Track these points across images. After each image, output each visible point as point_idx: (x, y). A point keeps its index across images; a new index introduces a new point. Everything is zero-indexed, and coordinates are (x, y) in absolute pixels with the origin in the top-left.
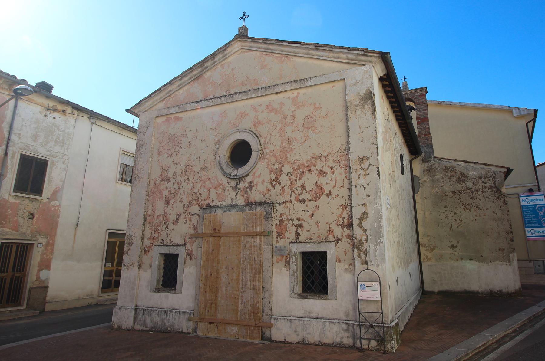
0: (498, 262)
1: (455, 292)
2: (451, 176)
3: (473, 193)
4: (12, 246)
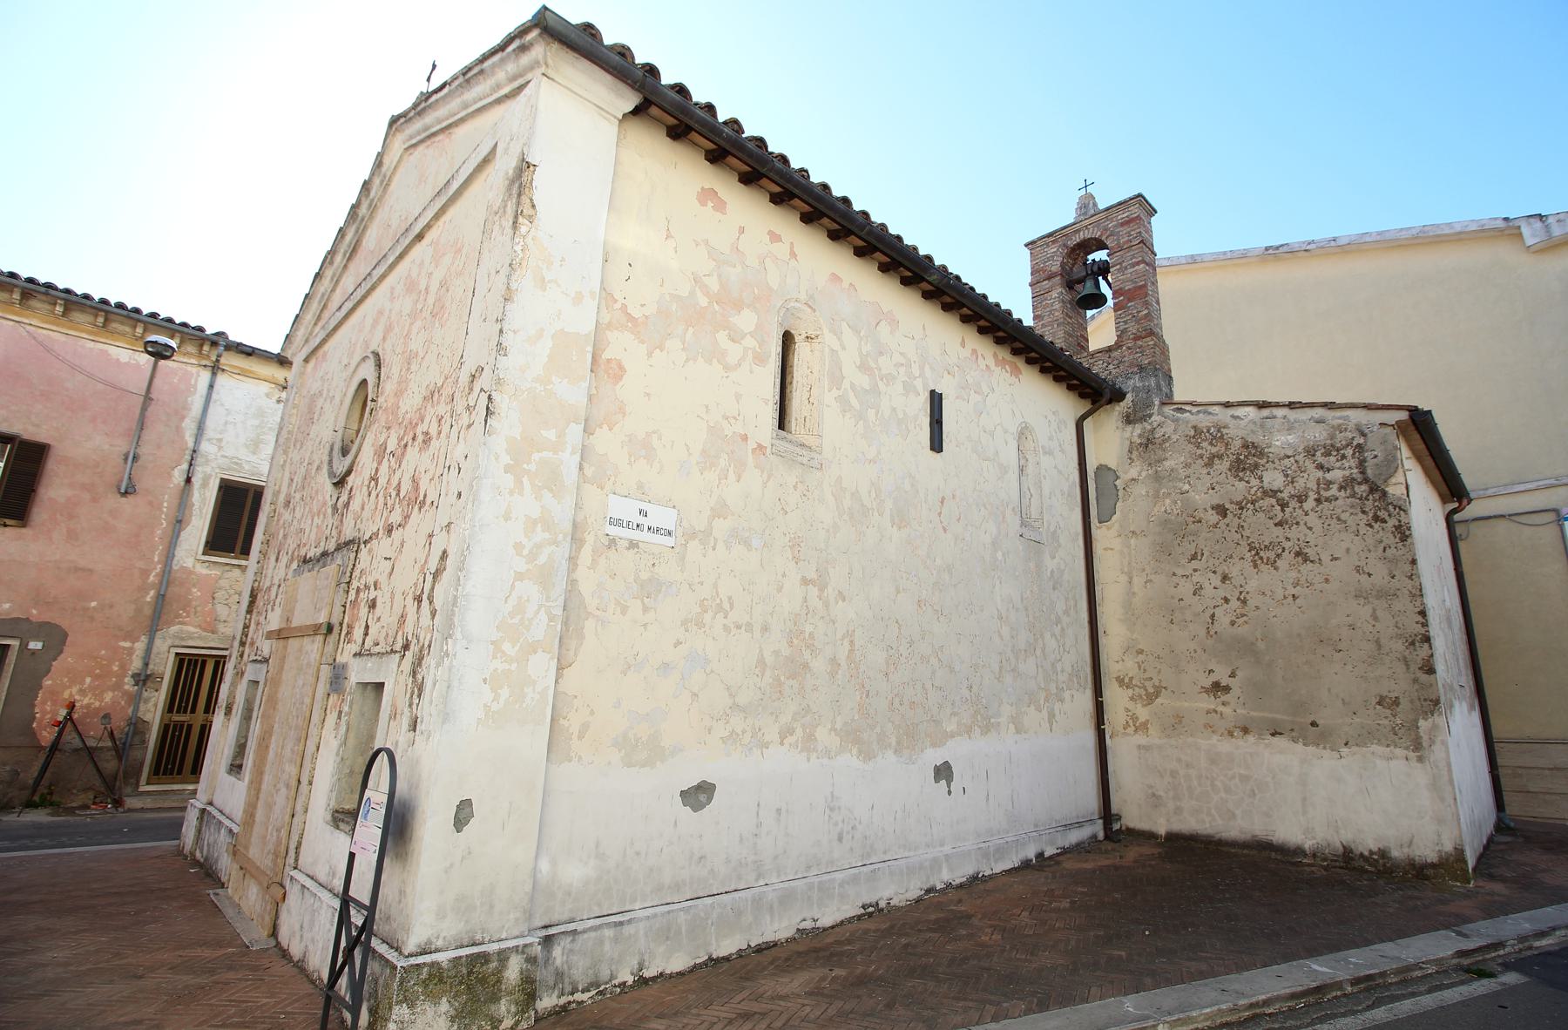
0: (1374, 748)
1: (1221, 843)
2: (1213, 457)
3: (1283, 506)
4: (204, 662)
